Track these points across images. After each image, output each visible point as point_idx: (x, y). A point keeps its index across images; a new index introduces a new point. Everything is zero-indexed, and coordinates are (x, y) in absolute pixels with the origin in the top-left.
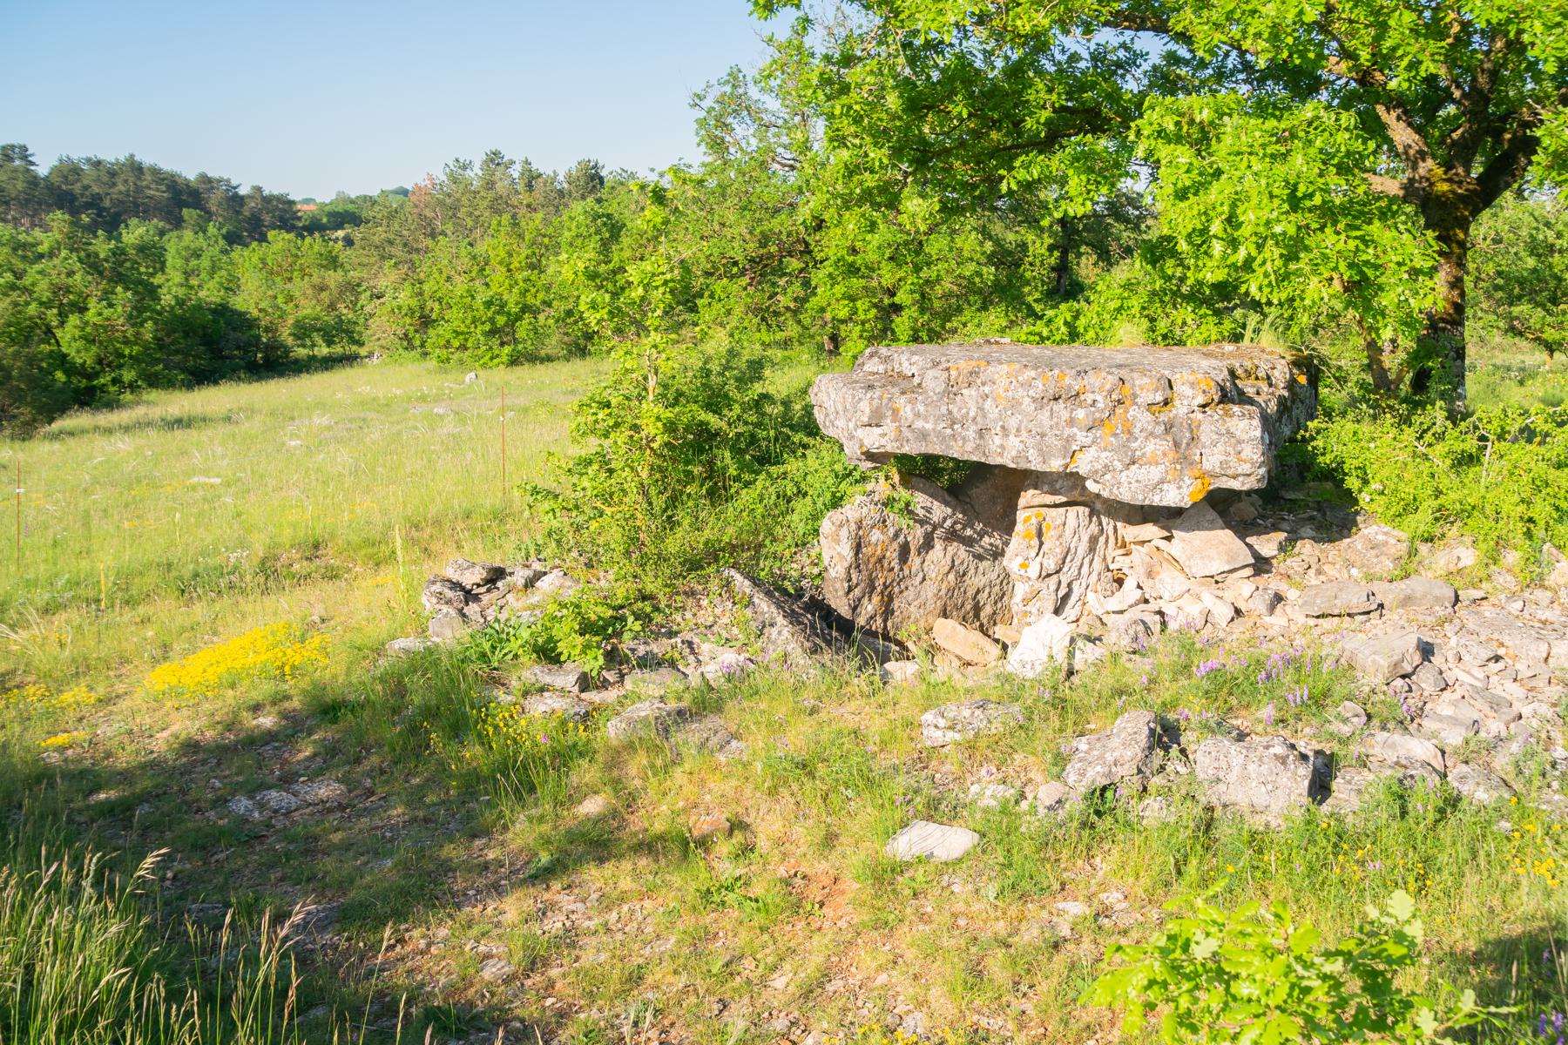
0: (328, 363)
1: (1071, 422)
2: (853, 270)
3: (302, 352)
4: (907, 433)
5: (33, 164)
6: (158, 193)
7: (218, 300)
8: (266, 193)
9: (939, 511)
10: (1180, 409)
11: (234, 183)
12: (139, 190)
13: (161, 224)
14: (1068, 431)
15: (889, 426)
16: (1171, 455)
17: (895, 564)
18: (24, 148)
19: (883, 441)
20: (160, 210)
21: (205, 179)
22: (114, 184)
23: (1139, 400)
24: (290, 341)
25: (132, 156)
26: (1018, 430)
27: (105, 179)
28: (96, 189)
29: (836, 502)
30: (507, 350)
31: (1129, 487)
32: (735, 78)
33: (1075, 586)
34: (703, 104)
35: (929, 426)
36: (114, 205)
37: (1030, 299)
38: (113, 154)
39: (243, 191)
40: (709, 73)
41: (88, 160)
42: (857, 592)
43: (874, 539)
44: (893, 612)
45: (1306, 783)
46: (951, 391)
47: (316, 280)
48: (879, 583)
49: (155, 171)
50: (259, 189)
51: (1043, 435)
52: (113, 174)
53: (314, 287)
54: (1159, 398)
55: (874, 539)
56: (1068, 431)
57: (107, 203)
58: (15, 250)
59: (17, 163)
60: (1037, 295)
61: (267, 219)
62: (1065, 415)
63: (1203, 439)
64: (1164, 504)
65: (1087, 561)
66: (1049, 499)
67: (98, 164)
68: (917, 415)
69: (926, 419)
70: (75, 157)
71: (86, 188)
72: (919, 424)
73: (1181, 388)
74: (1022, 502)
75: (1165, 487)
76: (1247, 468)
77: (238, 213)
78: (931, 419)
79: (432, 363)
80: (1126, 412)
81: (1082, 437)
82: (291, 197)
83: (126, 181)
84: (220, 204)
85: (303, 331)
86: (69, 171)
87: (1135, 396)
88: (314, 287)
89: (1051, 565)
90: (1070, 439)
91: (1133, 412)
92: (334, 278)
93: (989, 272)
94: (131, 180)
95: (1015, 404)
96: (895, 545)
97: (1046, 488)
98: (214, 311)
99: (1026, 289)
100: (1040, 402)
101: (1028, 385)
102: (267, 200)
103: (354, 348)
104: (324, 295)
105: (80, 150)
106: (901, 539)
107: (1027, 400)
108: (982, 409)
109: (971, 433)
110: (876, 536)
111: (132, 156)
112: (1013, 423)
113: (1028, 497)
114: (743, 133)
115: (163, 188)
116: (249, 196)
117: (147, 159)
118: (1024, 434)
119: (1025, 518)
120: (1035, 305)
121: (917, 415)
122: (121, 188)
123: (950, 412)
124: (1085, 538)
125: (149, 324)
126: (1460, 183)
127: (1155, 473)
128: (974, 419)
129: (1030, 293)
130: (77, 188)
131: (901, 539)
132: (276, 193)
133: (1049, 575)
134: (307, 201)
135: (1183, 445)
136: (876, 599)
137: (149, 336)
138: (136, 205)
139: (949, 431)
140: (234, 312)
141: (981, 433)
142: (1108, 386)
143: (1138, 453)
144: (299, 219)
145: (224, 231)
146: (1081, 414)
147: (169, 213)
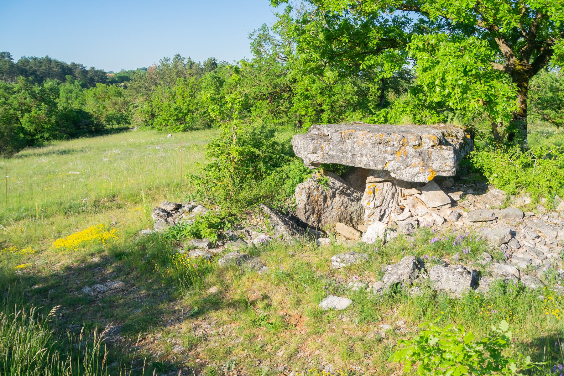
0: (118, 131)
1: (385, 152)
2: (307, 97)
3: (109, 127)
4: (326, 156)
5: (12, 59)
6: (56, 69)
7: (78, 108)
8: (96, 69)
9: (338, 184)
10: (424, 147)
11: (84, 66)
12: (50, 68)
13: (58, 81)
14: (384, 155)
15: (320, 153)
16: (421, 164)
17: (322, 203)
18: (9, 53)
19: (318, 159)
20: (58, 76)
21: (74, 64)
22: (41, 66)
23: (409, 144)
24: (104, 123)
25: (47, 56)
26: (366, 155)
27: (38, 64)
28: (34, 68)
29: (301, 181)
30: (182, 126)
31: (406, 175)
32: (264, 28)
33: (387, 211)
34: (253, 37)
35: (334, 153)
36: (41, 74)
37: (370, 108)
38: (41, 55)
39: (87, 69)
40: (255, 26)
41: (32, 58)
42: (308, 213)
43: (314, 194)
44: (321, 220)
45: (470, 282)
46: (342, 141)
47: (114, 101)
48: (316, 210)
49: (56, 62)
50: (93, 68)
51: (375, 157)
52: (40, 63)
53: (113, 103)
54: (417, 143)
55: (314, 194)
56: (384, 155)
57: (38, 73)
58: (5, 90)
59: (6, 58)
60: (373, 106)
61: (96, 79)
62: (383, 149)
63: (433, 158)
64: (419, 181)
65: (391, 202)
66: (377, 180)
67: (35, 59)
68: (330, 149)
69: (333, 151)
70: (27, 56)
71: (31, 67)
72: (330, 153)
73: (425, 140)
74: (368, 181)
75: (419, 175)
76: (448, 168)
77: (86, 76)
78: (335, 151)
79: (155, 131)
80: (405, 148)
81: (389, 157)
82: (105, 71)
83: (45, 65)
84: (79, 73)
85: (109, 119)
86: (25, 61)
87: (408, 142)
88: (113, 103)
89: (378, 203)
90: (385, 158)
91: (407, 148)
92: (120, 100)
93: (356, 98)
94: (47, 65)
95: (365, 145)
96: (322, 196)
97: (376, 176)
98: (77, 112)
99: (369, 104)
100: (374, 145)
101: (370, 138)
102: (96, 72)
103: (127, 125)
104: (117, 106)
105: (29, 54)
106: (324, 194)
107: (369, 144)
108: (353, 147)
109: (349, 156)
110: (315, 193)
111: (47, 56)
112: (364, 152)
113: (370, 179)
114: (267, 48)
115: (59, 68)
116: (90, 71)
117: (53, 57)
118: (368, 156)
119: (369, 187)
120: (372, 110)
121: (330, 149)
122: (44, 68)
123: (342, 148)
124: (390, 194)
125: (54, 117)
126: (525, 66)
127: (416, 170)
128: (350, 151)
129: (370, 106)
130: (28, 68)
131: (324, 194)
132: (99, 69)
133: (377, 207)
134: (110, 72)
135: (426, 160)
136: (315, 216)
137: (53, 121)
138: (49, 74)
139: (341, 155)
140: (84, 112)
141: (353, 156)
142: (399, 139)
143: (409, 163)
144: (108, 79)
145: (81, 83)
146: (389, 149)
147: (61, 77)
